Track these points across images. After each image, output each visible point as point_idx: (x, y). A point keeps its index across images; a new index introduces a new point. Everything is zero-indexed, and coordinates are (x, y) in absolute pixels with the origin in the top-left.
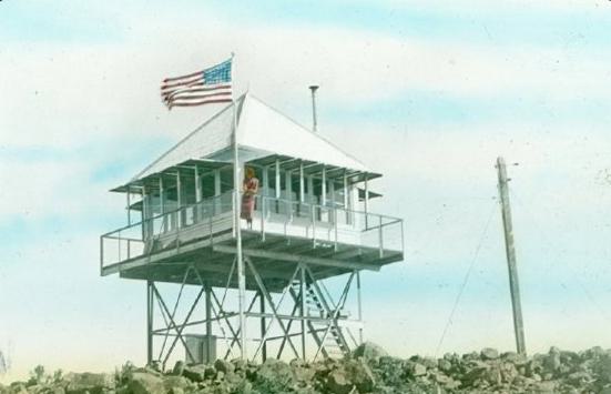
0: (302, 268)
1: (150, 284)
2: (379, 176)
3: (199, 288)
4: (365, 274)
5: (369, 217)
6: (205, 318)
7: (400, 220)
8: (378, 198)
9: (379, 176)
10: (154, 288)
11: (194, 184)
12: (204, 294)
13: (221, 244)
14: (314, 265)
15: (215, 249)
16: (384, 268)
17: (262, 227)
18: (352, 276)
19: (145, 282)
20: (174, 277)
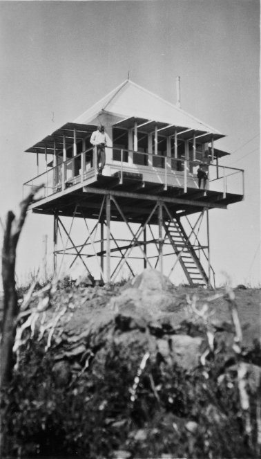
0: (160, 205)
1: (57, 218)
2: (229, 154)
3: (97, 221)
4: (215, 212)
5: (219, 168)
6: (120, 246)
7: (243, 171)
8: (228, 156)
9: (229, 154)
10: (59, 219)
11: (75, 207)
12: (100, 225)
13: (88, 186)
14: (171, 203)
15: (84, 190)
16: (230, 206)
17: (170, 275)
18: (203, 214)
19: (52, 217)
20: (248, 429)
